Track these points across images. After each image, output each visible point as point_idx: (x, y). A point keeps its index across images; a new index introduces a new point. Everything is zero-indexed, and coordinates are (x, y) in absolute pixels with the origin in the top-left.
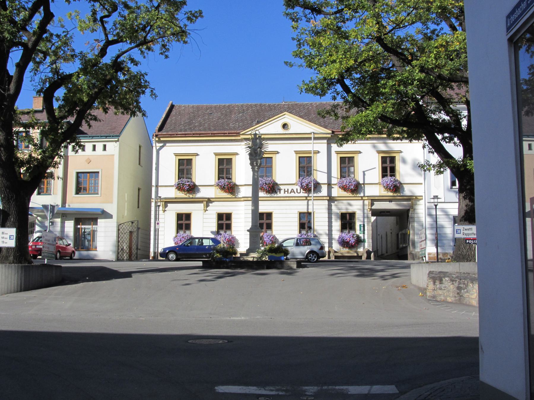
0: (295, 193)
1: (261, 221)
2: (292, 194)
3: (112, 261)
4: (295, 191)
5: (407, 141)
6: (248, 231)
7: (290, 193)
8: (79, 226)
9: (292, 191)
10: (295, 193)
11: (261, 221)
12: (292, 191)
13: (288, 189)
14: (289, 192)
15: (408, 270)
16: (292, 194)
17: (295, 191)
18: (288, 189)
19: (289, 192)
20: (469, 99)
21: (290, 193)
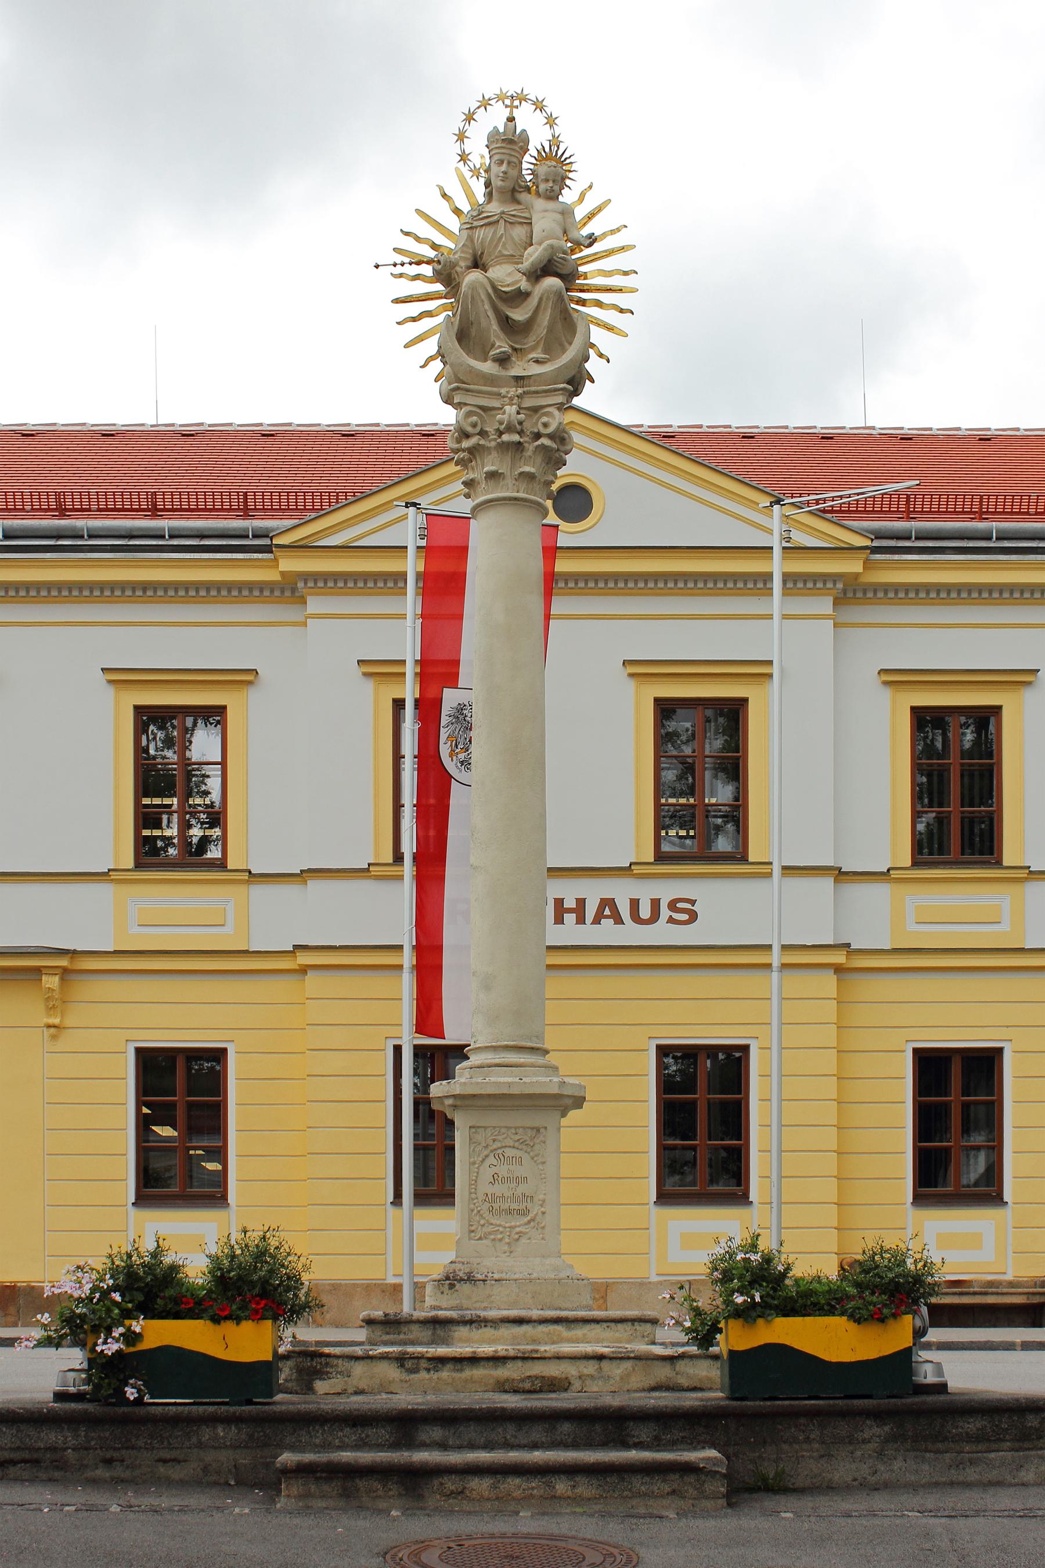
0: (619, 921)
1: (776, 949)
2: (607, 933)
3: (738, 788)
4: (625, 911)
5: (414, 943)
6: (57, 1349)
7: (597, 921)
8: (192, 1113)
9: (607, 912)
10: (619, 921)
11: (776, 949)
12: (607, 912)
13: (581, 903)
14: (590, 913)
15: (769, 553)
16: (607, 933)
17: (625, 911)
18: (559, 920)
19: (590, 913)
20: (18, 1349)
21: (597, 921)
